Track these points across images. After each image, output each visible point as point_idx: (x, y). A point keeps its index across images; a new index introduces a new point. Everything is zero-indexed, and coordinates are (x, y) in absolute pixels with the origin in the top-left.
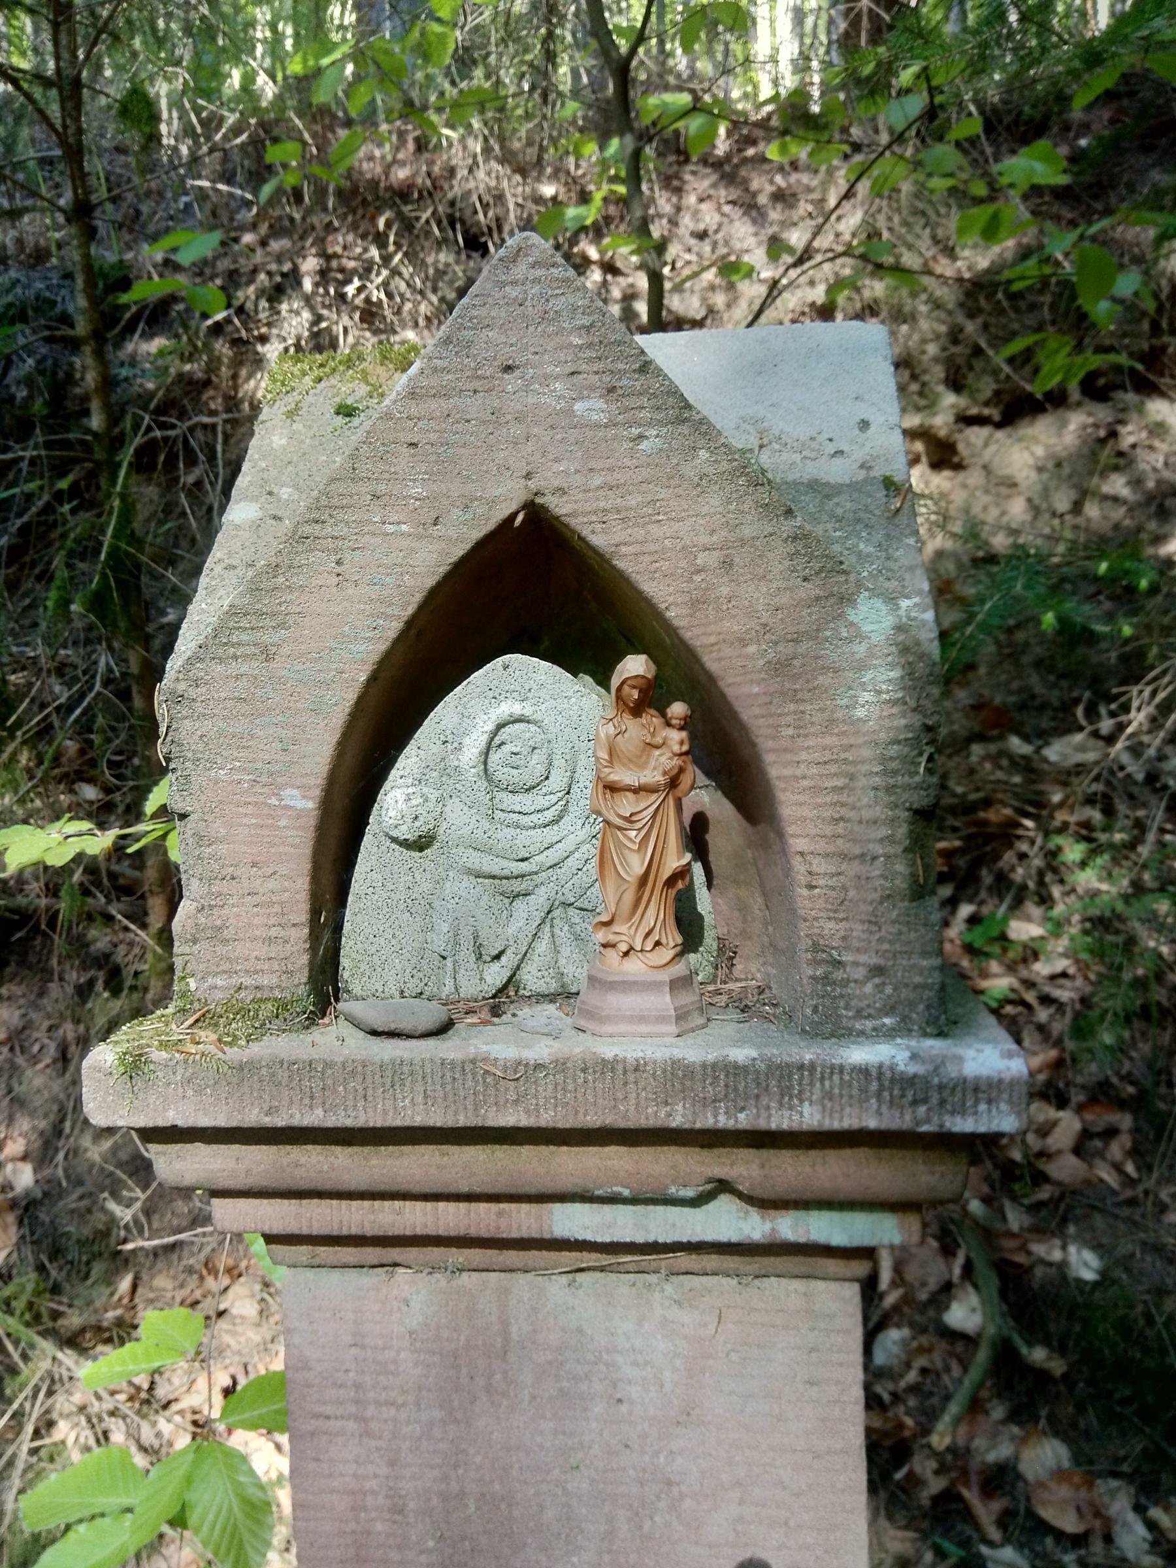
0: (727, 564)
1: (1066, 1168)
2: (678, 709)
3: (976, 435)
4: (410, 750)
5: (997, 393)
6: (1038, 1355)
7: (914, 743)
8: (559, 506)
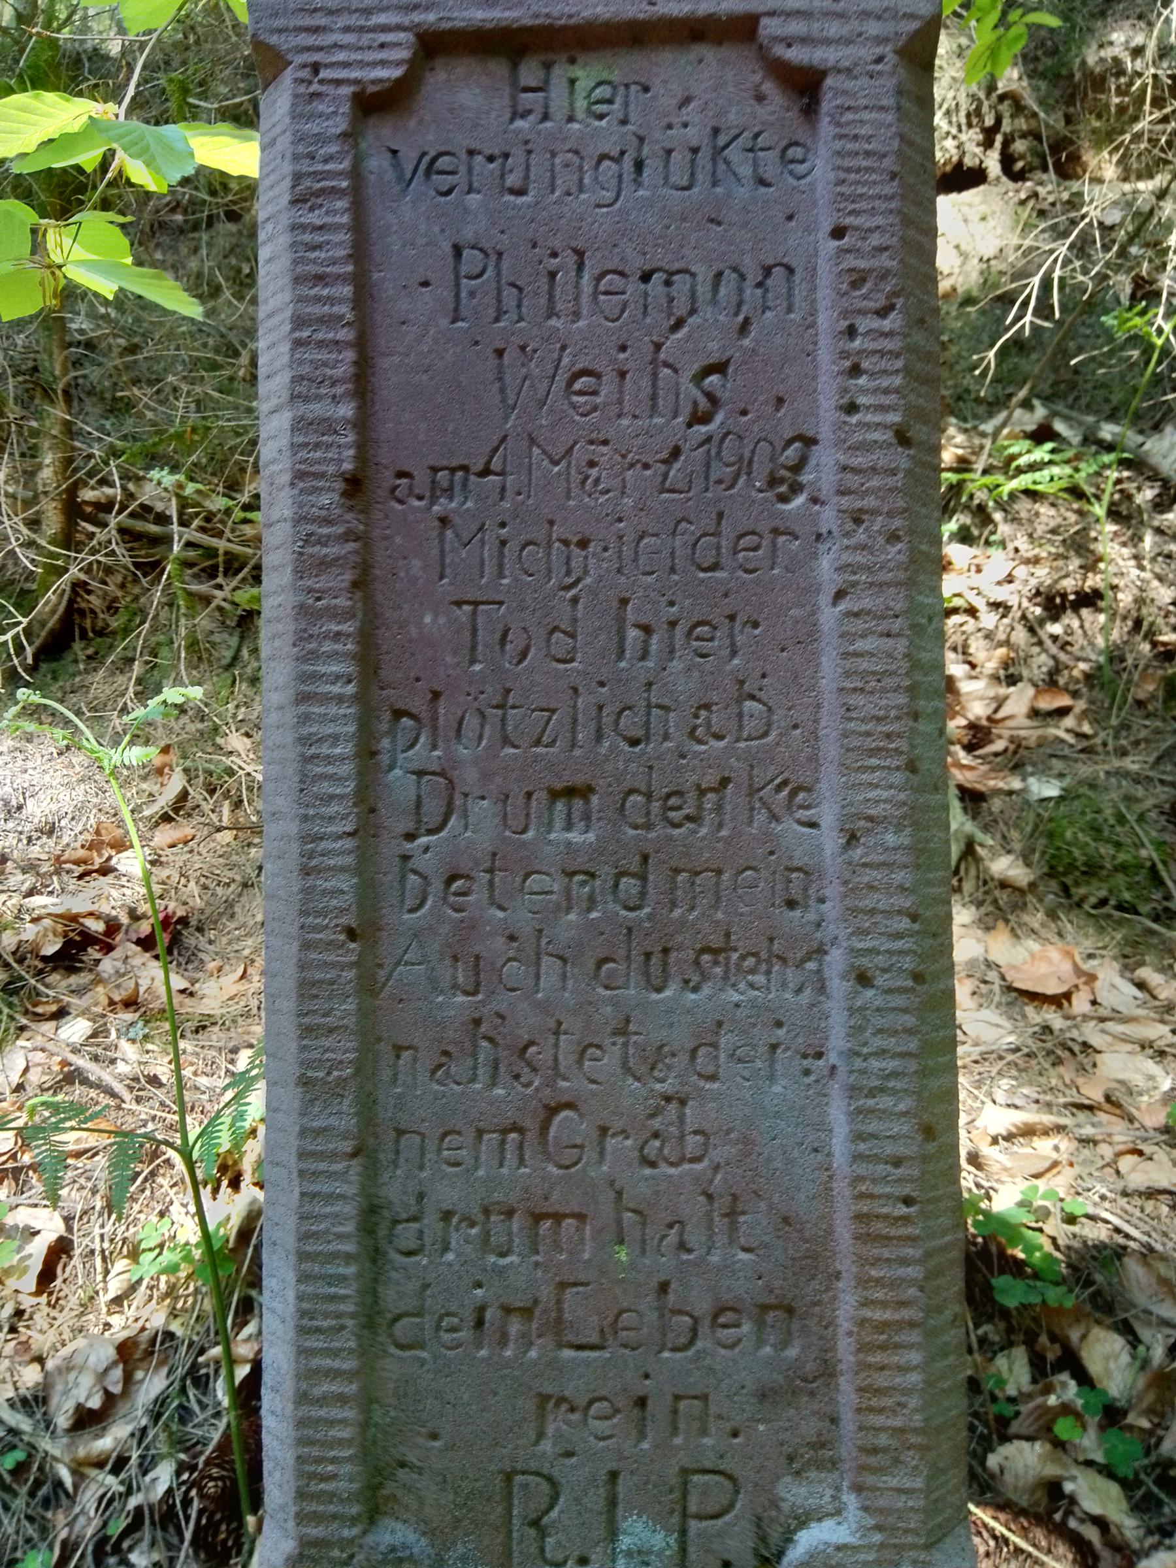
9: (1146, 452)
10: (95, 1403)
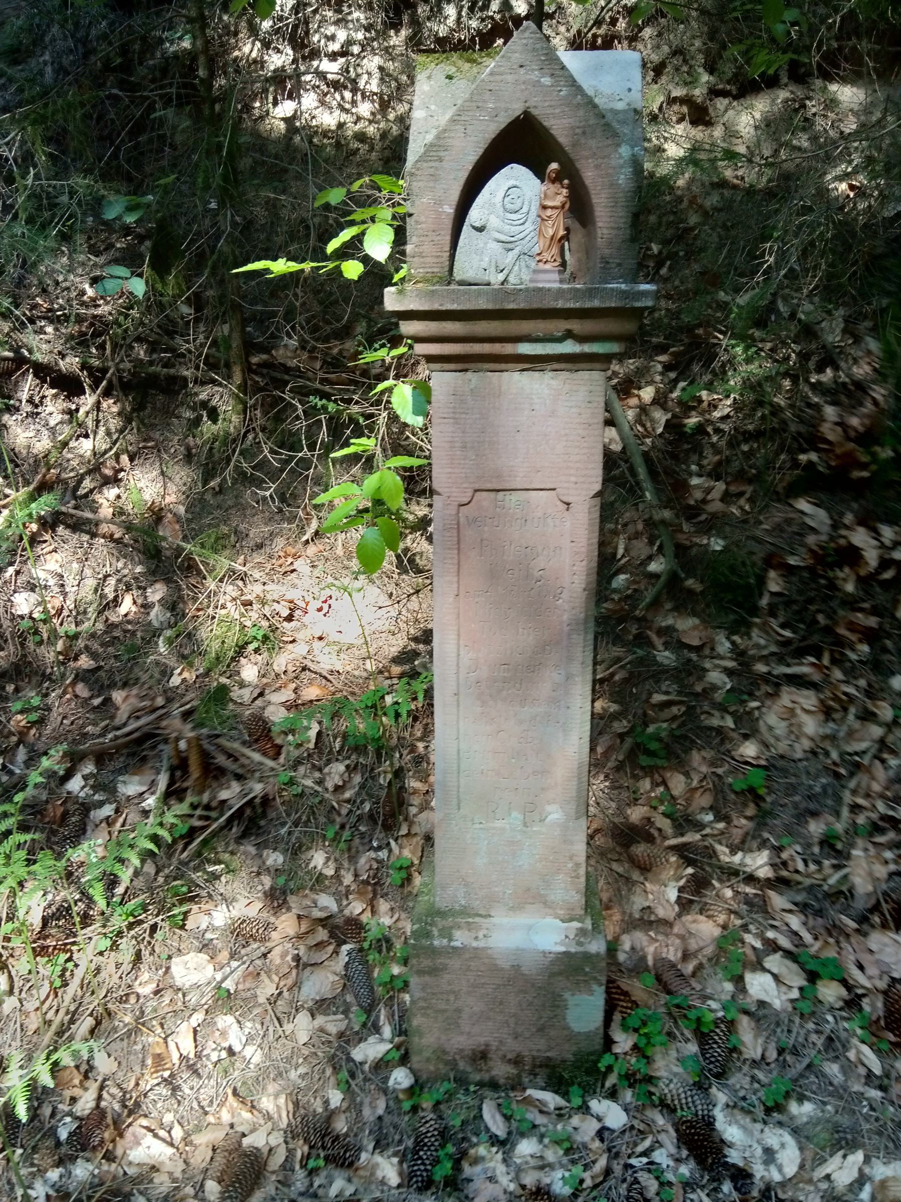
0: (584, 133)
1: (716, 506)
2: (566, 182)
3: (721, 103)
4: (480, 196)
5: (736, 75)
6: (690, 583)
7: (634, 192)
8: (535, 112)
9: (822, 329)
10: (340, 783)
